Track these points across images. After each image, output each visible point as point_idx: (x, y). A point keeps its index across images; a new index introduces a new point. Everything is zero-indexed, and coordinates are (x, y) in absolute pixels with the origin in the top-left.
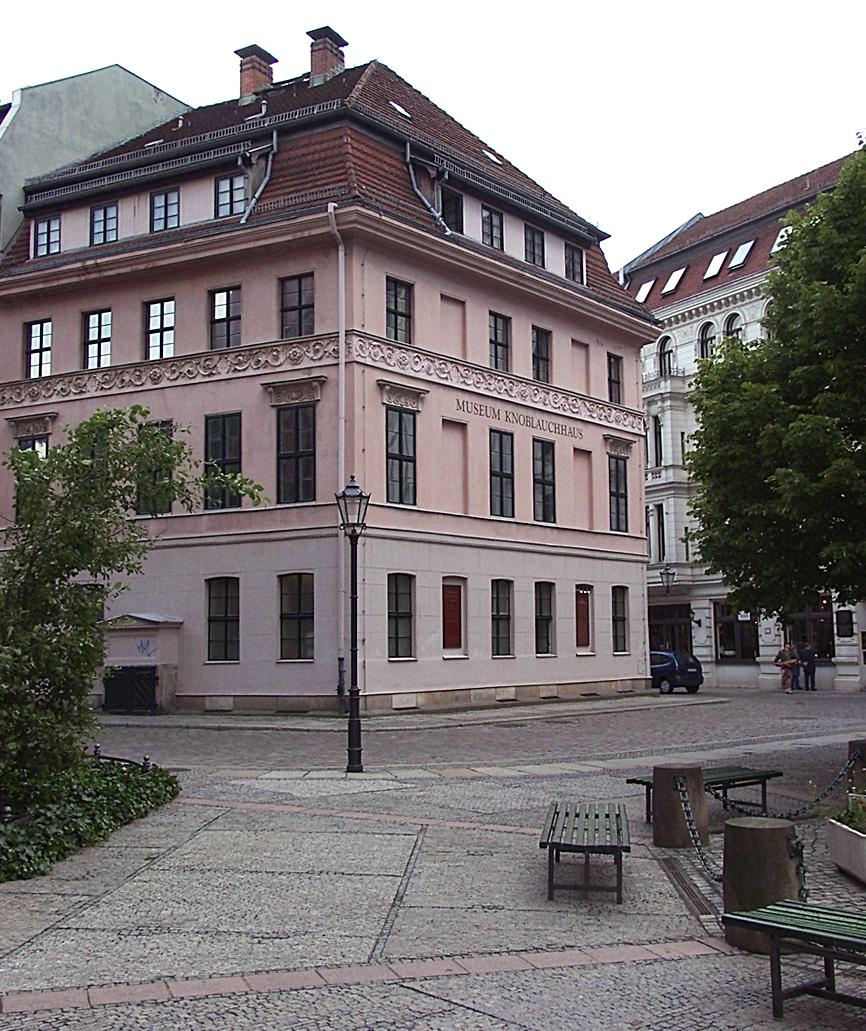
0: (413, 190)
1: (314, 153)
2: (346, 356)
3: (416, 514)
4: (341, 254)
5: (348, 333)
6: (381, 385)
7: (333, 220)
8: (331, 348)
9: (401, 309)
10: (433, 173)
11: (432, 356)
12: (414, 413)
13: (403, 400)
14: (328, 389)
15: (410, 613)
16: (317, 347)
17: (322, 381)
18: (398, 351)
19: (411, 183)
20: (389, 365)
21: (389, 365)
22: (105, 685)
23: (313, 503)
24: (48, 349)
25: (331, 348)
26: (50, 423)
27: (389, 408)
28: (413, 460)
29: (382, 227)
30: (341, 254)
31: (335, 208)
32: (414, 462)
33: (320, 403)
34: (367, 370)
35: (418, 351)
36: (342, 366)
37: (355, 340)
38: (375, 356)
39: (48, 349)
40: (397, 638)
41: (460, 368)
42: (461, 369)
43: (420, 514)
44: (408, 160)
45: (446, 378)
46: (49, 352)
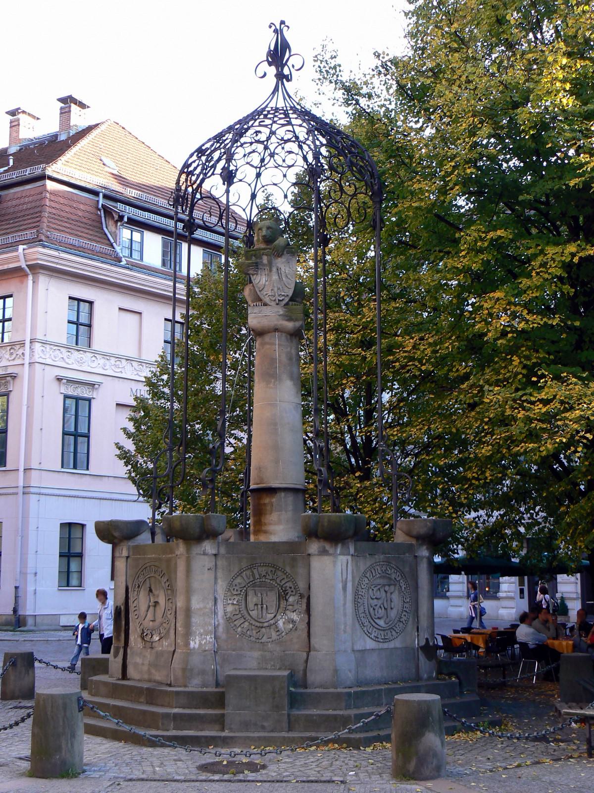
0: (103, 229)
1: (24, 204)
2: (30, 358)
3: (88, 476)
4: (30, 282)
5: (32, 341)
6: (59, 380)
7: (22, 257)
8: (20, 352)
9: (84, 319)
10: (116, 217)
11: (106, 355)
12: (89, 400)
13: (79, 390)
14: (17, 381)
15: (82, 553)
16: (12, 351)
17: (14, 377)
18: (77, 353)
19: (102, 223)
20: (68, 364)
21: (68, 364)
22: (561, 624)
23: (4, 469)
24: (10, 320)
25: (20, 352)
26: (12, 382)
27: (66, 397)
28: (87, 436)
29: (60, 262)
30: (30, 282)
31: (24, 249)
32: (88, 437)
33: (12, 393)
34: (47, 367)
35: (95, 353)
36: (27, 366)
37: (37, 346)
38: (55, 357)
39: (10, 320)
40: (68, 572)
41: (134, 363)
42: (135, 364)
43: (92, 477)
44: (100, 206)
45: (121, 372)
46: (10, 322)
